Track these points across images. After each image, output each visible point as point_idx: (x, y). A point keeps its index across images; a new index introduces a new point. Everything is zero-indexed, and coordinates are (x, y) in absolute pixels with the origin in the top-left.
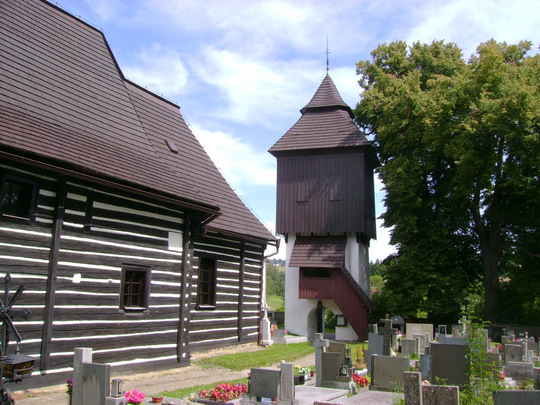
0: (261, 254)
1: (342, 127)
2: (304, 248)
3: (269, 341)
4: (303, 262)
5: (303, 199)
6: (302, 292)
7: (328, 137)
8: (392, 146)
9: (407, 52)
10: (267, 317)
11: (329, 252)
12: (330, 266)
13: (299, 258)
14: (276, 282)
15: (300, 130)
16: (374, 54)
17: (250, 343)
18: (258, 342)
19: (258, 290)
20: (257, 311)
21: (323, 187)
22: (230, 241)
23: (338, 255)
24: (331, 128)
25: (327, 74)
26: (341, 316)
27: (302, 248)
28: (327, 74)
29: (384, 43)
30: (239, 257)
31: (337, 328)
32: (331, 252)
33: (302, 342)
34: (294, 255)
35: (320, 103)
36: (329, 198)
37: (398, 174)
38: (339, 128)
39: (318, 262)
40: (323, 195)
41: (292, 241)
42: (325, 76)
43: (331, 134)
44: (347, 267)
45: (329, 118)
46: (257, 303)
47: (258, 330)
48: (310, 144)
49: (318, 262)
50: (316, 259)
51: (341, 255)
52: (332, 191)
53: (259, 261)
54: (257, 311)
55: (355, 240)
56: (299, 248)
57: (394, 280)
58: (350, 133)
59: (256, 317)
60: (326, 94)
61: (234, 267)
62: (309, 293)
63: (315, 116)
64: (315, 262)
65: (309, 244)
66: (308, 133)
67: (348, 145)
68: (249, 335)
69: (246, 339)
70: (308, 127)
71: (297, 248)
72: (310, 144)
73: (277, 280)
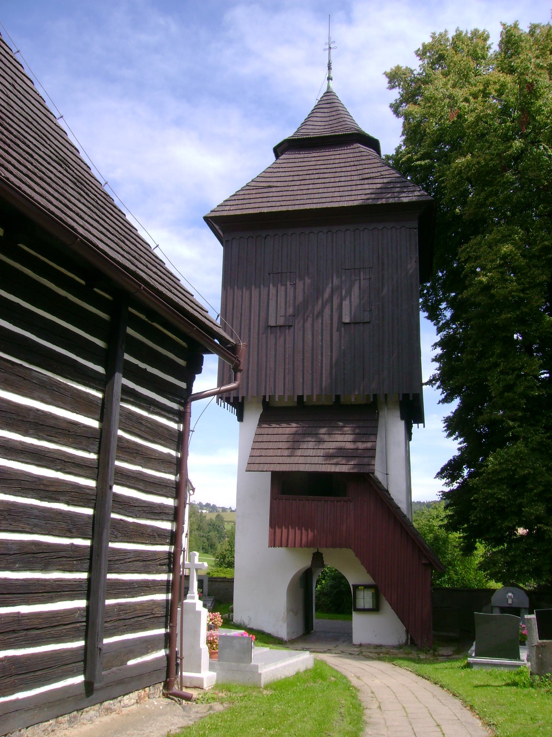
0: (183, 385)
1: (367, 171)
2: (280, 431)
3: (203, 673)
4: (281, 460)
5: (281, 322)
6: (278, 531)
7: (337, 189)
8: (486, 199)
9: (489, 48)
10: (197, 596)
11: (340, 438)
12: (344, 469)
13: (271, 453)
14: (202, 534)
15: (274, 179)
16: (422, 54)
17: (134, 695)
18: (167, 685)
19: (170, 502)
20: (163, 577)
21: (326, 295)
22: (63, 293)
23: (360, 445)
24: (343, 174)
25: (329, 87)
26: (367, 587)
27: (276, 431)
28: (329, 87)
29: (443, 31)
30: (100, 369)
31: (356, 618)
32: (343, 438)
33: (302, 669)
34: (257, 445)
35: (318, 130)
36: (340, 317)
37: (504, 257)
38: (359, 172)
39: (316, 460)
40: (327, 311)
41: (253, 417)
42: (325, 90)
43: (340, 185)
44: (379, 475)
45: (337, 157)
46: (166, 548)
47: (168, 640)
48: (297, 202)
49: (316, 460)
50: (311, 452)
51: (369, 445)
52: (346, 303)
53: (175, 406)
54: (163, 577)
55: (398, 413)
56: (270, 431)
57: (499, 500)
58: (385, 181)
59: (161, 597)
60: (328, 119)
61: (156, 536)
62: (294, 534)
63: (306, 155)
64: (309, 460)
65: (293, 421)
66: (293, 183)
67: (384, 201)
68: (131, 663)
69: (121, 682)
70: (292, 174)
71: (266, 431)
72: (297, 202)
73: (203, 530)
